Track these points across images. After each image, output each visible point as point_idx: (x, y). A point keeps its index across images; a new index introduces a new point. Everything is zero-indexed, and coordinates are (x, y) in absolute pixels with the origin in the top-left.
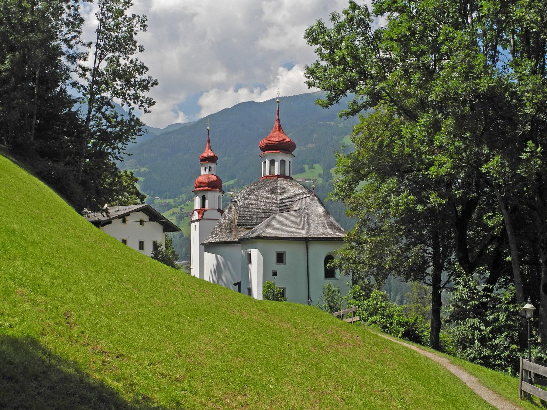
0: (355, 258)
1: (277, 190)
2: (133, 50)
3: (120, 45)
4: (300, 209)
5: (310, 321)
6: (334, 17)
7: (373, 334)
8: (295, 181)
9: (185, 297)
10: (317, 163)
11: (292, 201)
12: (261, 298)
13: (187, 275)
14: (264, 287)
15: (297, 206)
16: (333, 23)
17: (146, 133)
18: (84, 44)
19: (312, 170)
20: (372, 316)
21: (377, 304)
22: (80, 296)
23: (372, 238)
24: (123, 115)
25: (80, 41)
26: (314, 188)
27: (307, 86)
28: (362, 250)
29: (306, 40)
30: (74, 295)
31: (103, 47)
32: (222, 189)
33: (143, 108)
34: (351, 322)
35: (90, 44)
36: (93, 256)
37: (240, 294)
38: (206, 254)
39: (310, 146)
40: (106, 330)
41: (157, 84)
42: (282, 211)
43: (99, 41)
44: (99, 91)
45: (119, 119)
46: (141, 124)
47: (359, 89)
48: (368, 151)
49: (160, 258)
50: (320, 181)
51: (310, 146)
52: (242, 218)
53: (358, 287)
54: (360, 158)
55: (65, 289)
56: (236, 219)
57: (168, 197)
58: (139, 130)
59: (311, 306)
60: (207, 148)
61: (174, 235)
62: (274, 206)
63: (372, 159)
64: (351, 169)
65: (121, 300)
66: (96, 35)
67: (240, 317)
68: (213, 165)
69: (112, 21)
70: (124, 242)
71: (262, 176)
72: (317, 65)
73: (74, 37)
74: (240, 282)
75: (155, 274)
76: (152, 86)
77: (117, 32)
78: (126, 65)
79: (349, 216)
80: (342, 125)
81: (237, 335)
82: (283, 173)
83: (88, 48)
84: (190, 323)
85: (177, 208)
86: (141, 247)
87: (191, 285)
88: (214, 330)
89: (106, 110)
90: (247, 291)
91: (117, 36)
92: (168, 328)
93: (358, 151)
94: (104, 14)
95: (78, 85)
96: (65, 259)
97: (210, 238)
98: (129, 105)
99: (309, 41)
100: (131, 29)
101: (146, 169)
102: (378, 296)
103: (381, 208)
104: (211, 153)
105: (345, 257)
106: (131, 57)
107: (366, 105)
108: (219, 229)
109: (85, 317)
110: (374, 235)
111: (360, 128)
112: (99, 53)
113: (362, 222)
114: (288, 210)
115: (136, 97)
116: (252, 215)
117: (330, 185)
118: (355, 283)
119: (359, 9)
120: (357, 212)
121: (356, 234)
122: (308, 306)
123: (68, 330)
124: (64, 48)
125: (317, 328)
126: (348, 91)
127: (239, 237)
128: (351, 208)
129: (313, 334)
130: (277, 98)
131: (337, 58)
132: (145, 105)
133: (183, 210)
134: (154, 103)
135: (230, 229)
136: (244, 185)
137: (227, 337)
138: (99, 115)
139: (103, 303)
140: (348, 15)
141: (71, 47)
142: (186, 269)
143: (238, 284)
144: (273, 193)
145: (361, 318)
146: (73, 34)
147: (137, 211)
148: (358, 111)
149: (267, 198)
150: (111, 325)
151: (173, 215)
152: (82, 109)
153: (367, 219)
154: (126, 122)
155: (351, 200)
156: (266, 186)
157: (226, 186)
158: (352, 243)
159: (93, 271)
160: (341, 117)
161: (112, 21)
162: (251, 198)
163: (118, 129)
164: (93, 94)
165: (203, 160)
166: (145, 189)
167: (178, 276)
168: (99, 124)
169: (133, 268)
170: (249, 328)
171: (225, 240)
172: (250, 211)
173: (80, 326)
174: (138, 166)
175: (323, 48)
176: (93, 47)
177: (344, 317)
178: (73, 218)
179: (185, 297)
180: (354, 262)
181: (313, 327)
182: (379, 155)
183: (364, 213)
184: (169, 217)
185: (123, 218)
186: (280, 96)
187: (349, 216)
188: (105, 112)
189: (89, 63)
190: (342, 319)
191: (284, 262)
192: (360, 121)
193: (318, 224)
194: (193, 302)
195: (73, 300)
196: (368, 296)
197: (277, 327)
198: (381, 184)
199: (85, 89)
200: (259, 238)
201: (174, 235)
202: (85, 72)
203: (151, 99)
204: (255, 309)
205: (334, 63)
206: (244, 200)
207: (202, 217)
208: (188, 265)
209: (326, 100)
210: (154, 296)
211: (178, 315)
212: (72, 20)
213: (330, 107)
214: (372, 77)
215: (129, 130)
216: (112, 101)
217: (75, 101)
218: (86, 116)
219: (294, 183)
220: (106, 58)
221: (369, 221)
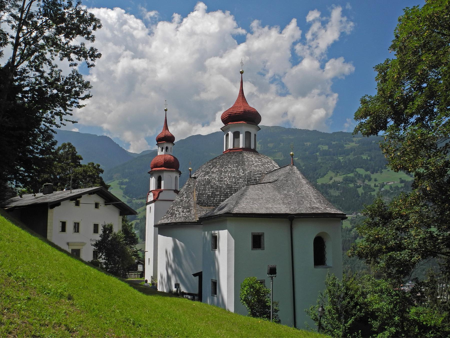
1: (243, 162)
11: (262, 175)
32: (179, 169)
38: (160, 237)
52: (202, 194)
56: (195, 196)
68: (170, 146)
71: (225, 150)
82: (248, 146)
97: (165, 218)
101: (127, 180)
116: (215, 191)
127: (199, 215)
135: (188, 207)
144: (239, 165)
149: (232, 172)
162: (213, 172)
171: (182, 220)
172: (212, 187)
185: (76, 199)
191: (264, 247)
193: (303, 197)
200: (229, 215)
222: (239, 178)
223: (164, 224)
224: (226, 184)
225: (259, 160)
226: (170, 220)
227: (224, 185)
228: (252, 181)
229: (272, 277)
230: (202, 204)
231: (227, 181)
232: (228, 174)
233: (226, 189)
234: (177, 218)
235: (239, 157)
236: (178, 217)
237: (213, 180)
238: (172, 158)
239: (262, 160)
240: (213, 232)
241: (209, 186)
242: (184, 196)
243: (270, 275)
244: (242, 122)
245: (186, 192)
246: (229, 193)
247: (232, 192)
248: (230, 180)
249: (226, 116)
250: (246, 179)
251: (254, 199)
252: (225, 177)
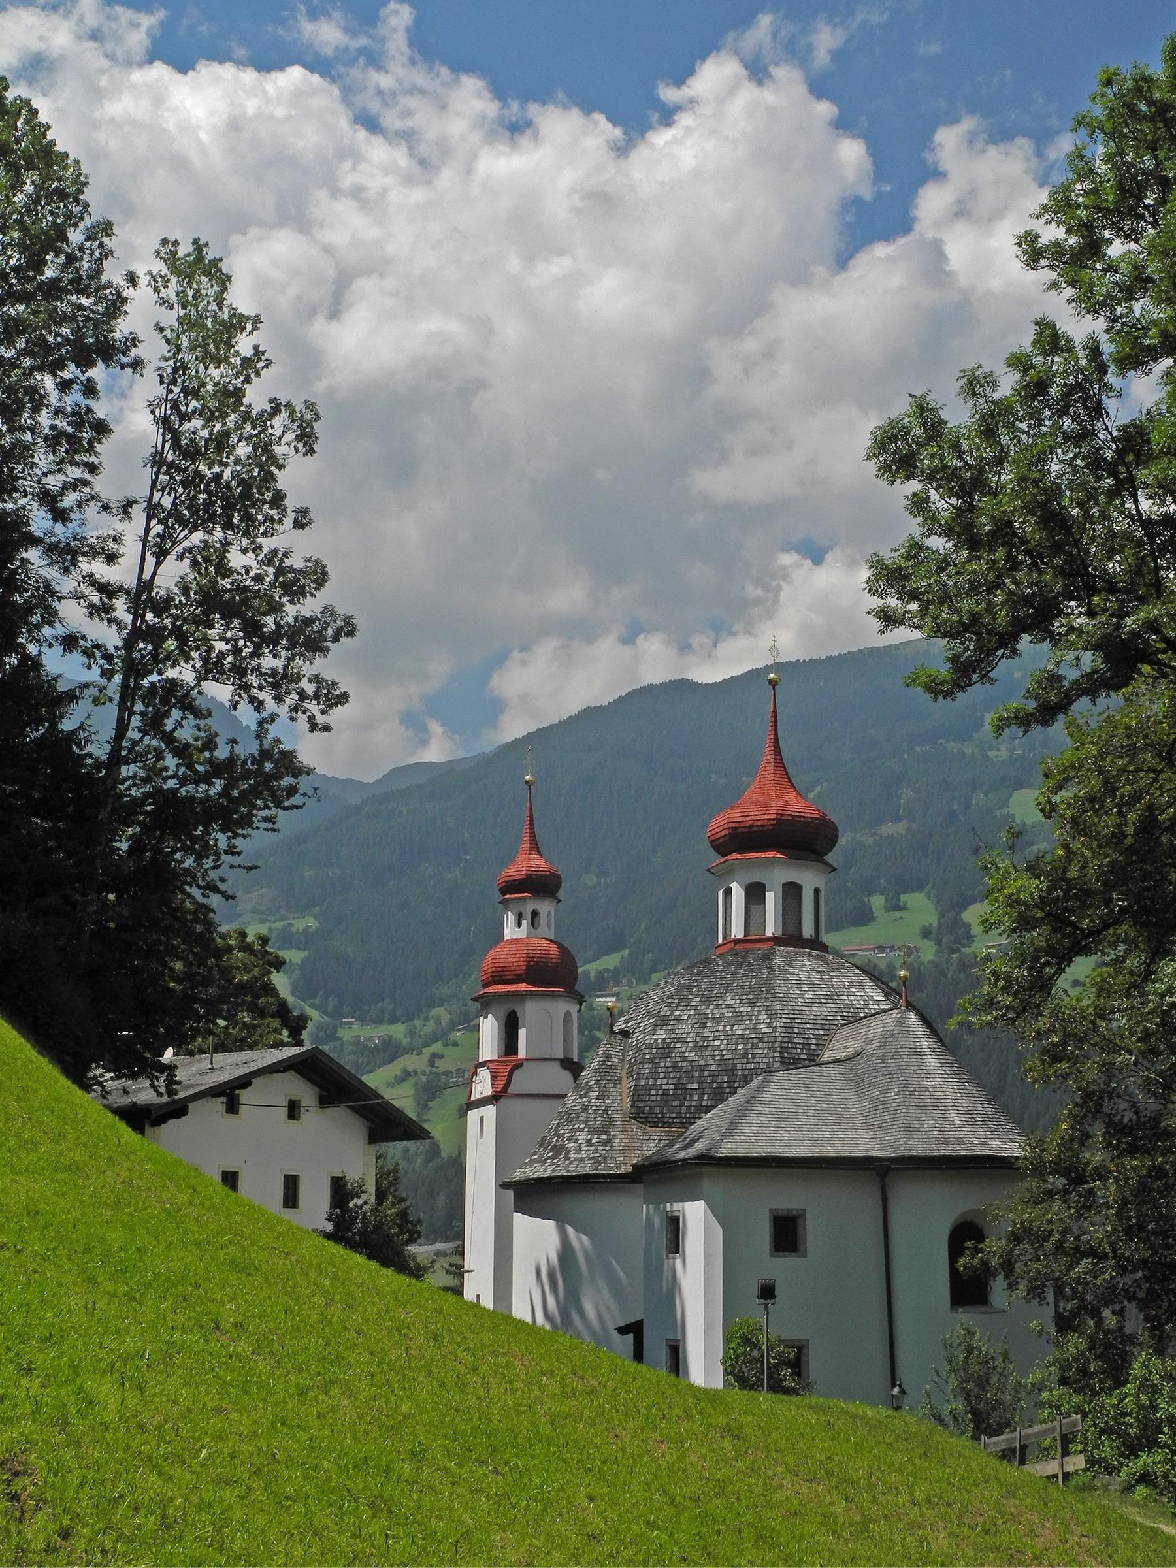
0: (1064, 1233)
1: (771, 988)
2: (272, 521)
3: (229, 507)
4: (857, 1054)
5: (900, 1471)
6: (974, 385)
7: (1142, 1526)
8: (839, 955)
9: (442, 1385)
10: (914, 891)
12: (718, 1382)
13: (451, 1298)
14: (727, 1340)
15: (843, 1045)
16: (970, 404)
17: (314, 799)
18: (106, 507)
19: (897, 914)
20: (1137, 1456)
21: (1154, 1408)
22: (63, 1391)
23: (1126, 1160)
24: (233, 742)
25: (93, 498)
26: (904, 980)
27: (877, 624)
28: (1088, 1204)
29: (873, 466)
30: (43, 1386)
31: (169, 515)
32: (579, 987)
33: (302, 719)
34: (1055, 1476)
35: (126, 508)
36: (116, 1237)
37: (642, 1367)
38: (518, 1218)
39: (889, 829)
40: (150, 1523)
41: (351, 633)
42: (792, 1063)
43: (157, 496)
44: (157, 660)
45: (222, 753)
46: (298, 771)
47: (1063, 630)
48: (1100, 846)
49: (355, 1234)
50: (928, 952)
51: (889, 829)
52: (647, 1089)
53: (1075, 1343)
54: (1073, 873)
55: (12, 1367)
56: (625, 1095)
57: (387, 1017)
58: (292, 791)
59: (902, 1412)
60: (525, 846)
61: (406, 1151)
62: (762, 1048)
63: (1116, 877)
64: (1040, 915)
65: (211, 1401)
66: (147, 473)
67: (641, 1456)
68: (545, 907)
69: (204, 427)
70: (230, 1179)
71: (720, 941)
72: (915, 550)
73: (75, 485)
74: (641, 1322)
75: (337, 1297)
76: (336, 639)
77: (221, 463)
78: (247, 572)
79: (1035, 1081)
80: (1004, 753)
81: (629, 1529)
82: (792, 929)
83: (121, 520)
84: (459, 1484)
85: (420, 1053)
86: (291, 1197)
87: (465, 1338)
88: (544, 1510)
89: (179, 724)
90: (664, 1354)
91: (218, 477)
92: (381, 1505)
93: (1066, 847)
94: (175, 405)
95: (82, 642)
96: (19, 1252)
97: (534, 1161)
98: (259, 705)
99: (885, 469)
100: (264, 447)
101: (311, 923)
102: (1156, 1380)
103: (1155, 1052)
104: (539, 864)
105: (1027, 1231)
106: (267, 544)
107: (1092, 686)
109: (77, 1472)
110: (1132, 1151)
111: (1072, 766)
112: (158, 535)
113: (1085, 1102)
114: (813, 1059)
115: (280, 681)
116: (685, 1080)
117: (964, 966)
118: (1065, 1324)
119: (1070, 349)
120: (1064, 1065)
121: (1066, 1144)
122: (891, 1412)
123: (13, 1528)
124: (39, 521)
125: (929, 1501)
126: (1026, 638)
128: (1045, 1051)
129: (913, 1525)
130: (768, 669)
131: (985, 524)
132: (313, 707)
133: (438, 1062)
134: (344, 698)
135: (605, 1129)
136: (654, 970)
137: (592, 1537)
138: (155, 743)
139: (146, 1417)
140: (1025, 371)
141: (60, 515)
142: (447, 1272)
143: (634, 1329)
144: (757, 999)
145: (1092, 1462)
146: (76, 473)
147: (278, 1071)
148: (1064, 705)
149: (738, 1019)
150: (171, 1500)
151: (403, 1080)
152: (94, 724)
153: (1103, 1091)
154: (245, 763)
155: (1043, 1023)
156: (734, 974)
157: (593, 974)
158: (1051, 1179)
159: (114, 1295)
160: (999, 730)
161: (204, 427)
162: (679, 1020)
163: (218, 786)
164: (134, 669)
165: (510, 887)
166: (304, 990)
167: (418, 1306)
168: (155, 772)
169: (258, 1278)
170: (673, 1503)
171: (587, 1168)
172: (675, 1066)
173: (58, 1510)
174: (283, 912)
175: (932, 492)
176: (139, 514)
177: (1028, 1456)
178: (56, 1100)
179: (442, 1385)
180: (1057, 1248)
181: (912, 1494)
182: (1143, 861)
183: (1091, 1070)
184: (390, 1085)
186: (782, 659)
187: (1035, 1081)
188: (174, 730)
189: (122, 574)
190: (1022, 1462)
191: (801, 1247)
192: (1068, 740)
193: (923, 1109)
194: (472, 1401)
195: (38, 1405)
196: (1117, 1374)
197: (778, 1495)
198: (1153, 961)
199: (108, 657)
200: (707, 1161)
201: (406, 1151)
202: (110, 599)
203: (334, 685)
204: (697, 1427)
205: (973, 542)
206: (655, 1028)
207: (505, 1089)
208: (455, 1259)
209: (943, 670)
210: (332, 1383)
211: (414, 1454)
212: (69, 429)
213: (960, 696)
214: (1112, 588)
215: (254, 792)
216: (200, 693)
217: (71, 697)
218: (108, 748)
219: (834, 962)
220: (179, 549)
221: (1111, 1098)
222: (755, 1041)
223: (533, 1179)
224: (718, 1058)
225: (822, 980)
227: (712, 1062)
228: (794, 1051)
229: (766, 1306)
230: (646, 1118)
231: (722, 1049)
232: (725, 1026)
233: (716, 1073)
234: (570, 1163)
235: (760, 970)
236: (576, 1159)
237: (678, 1045)
238: (554, 950)
239: (832, 977)
240: (668, 1205)
241: (668, 1064)
242: (592, 1094)
243: (763, 1301)
244: (771, 854)
245: (597, 1082)
246: (725, 1085)
247: (736, 1085)
248: (730, 1046)
249: (723, 833)
250: (777, 1044)
251: (781, 1116)
252: (716, 1037)
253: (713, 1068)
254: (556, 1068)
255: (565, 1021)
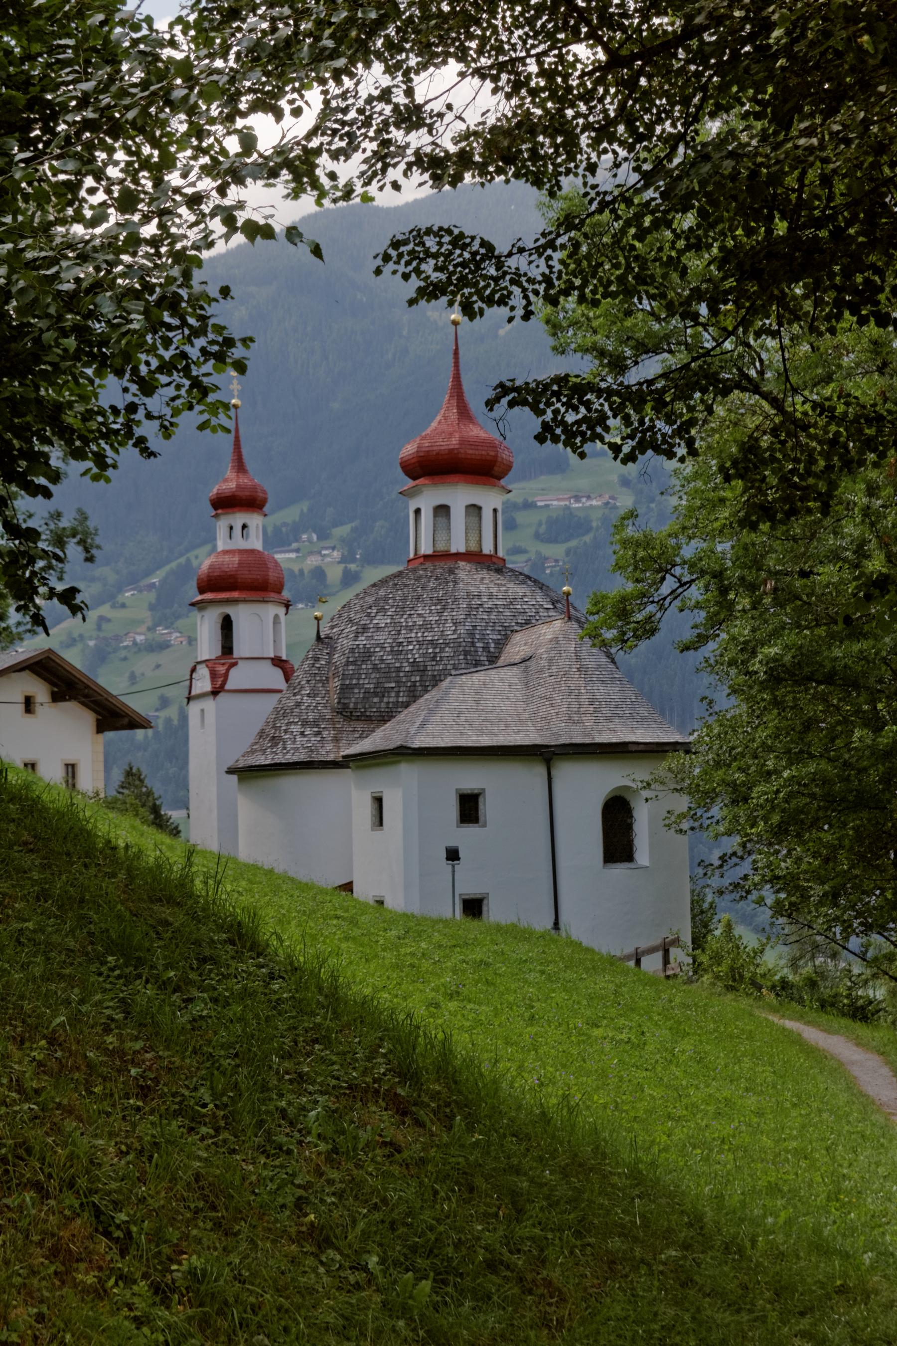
15: (518, 647)
71: (412, 556)
82: (473, 547)
108: (282, 724)
116: (384, 680)
133: (105, 626)
162: (378, 628)
172: (375, 668)
191: (481, 818)
206: (357, 635)
226: (270, 757)
231: (415, 653)
237: (377, 649)
245: (308, 681)
252: (409, 643)
253: (407, 669)
254: (268, 666)
255: (274, 623)
